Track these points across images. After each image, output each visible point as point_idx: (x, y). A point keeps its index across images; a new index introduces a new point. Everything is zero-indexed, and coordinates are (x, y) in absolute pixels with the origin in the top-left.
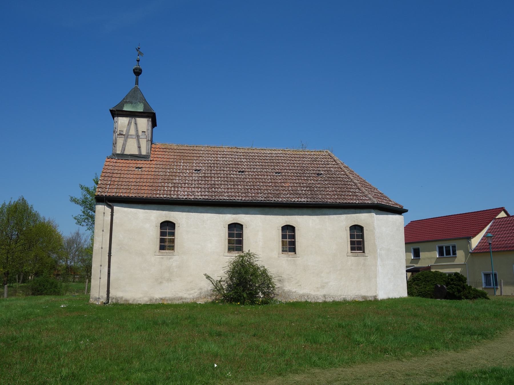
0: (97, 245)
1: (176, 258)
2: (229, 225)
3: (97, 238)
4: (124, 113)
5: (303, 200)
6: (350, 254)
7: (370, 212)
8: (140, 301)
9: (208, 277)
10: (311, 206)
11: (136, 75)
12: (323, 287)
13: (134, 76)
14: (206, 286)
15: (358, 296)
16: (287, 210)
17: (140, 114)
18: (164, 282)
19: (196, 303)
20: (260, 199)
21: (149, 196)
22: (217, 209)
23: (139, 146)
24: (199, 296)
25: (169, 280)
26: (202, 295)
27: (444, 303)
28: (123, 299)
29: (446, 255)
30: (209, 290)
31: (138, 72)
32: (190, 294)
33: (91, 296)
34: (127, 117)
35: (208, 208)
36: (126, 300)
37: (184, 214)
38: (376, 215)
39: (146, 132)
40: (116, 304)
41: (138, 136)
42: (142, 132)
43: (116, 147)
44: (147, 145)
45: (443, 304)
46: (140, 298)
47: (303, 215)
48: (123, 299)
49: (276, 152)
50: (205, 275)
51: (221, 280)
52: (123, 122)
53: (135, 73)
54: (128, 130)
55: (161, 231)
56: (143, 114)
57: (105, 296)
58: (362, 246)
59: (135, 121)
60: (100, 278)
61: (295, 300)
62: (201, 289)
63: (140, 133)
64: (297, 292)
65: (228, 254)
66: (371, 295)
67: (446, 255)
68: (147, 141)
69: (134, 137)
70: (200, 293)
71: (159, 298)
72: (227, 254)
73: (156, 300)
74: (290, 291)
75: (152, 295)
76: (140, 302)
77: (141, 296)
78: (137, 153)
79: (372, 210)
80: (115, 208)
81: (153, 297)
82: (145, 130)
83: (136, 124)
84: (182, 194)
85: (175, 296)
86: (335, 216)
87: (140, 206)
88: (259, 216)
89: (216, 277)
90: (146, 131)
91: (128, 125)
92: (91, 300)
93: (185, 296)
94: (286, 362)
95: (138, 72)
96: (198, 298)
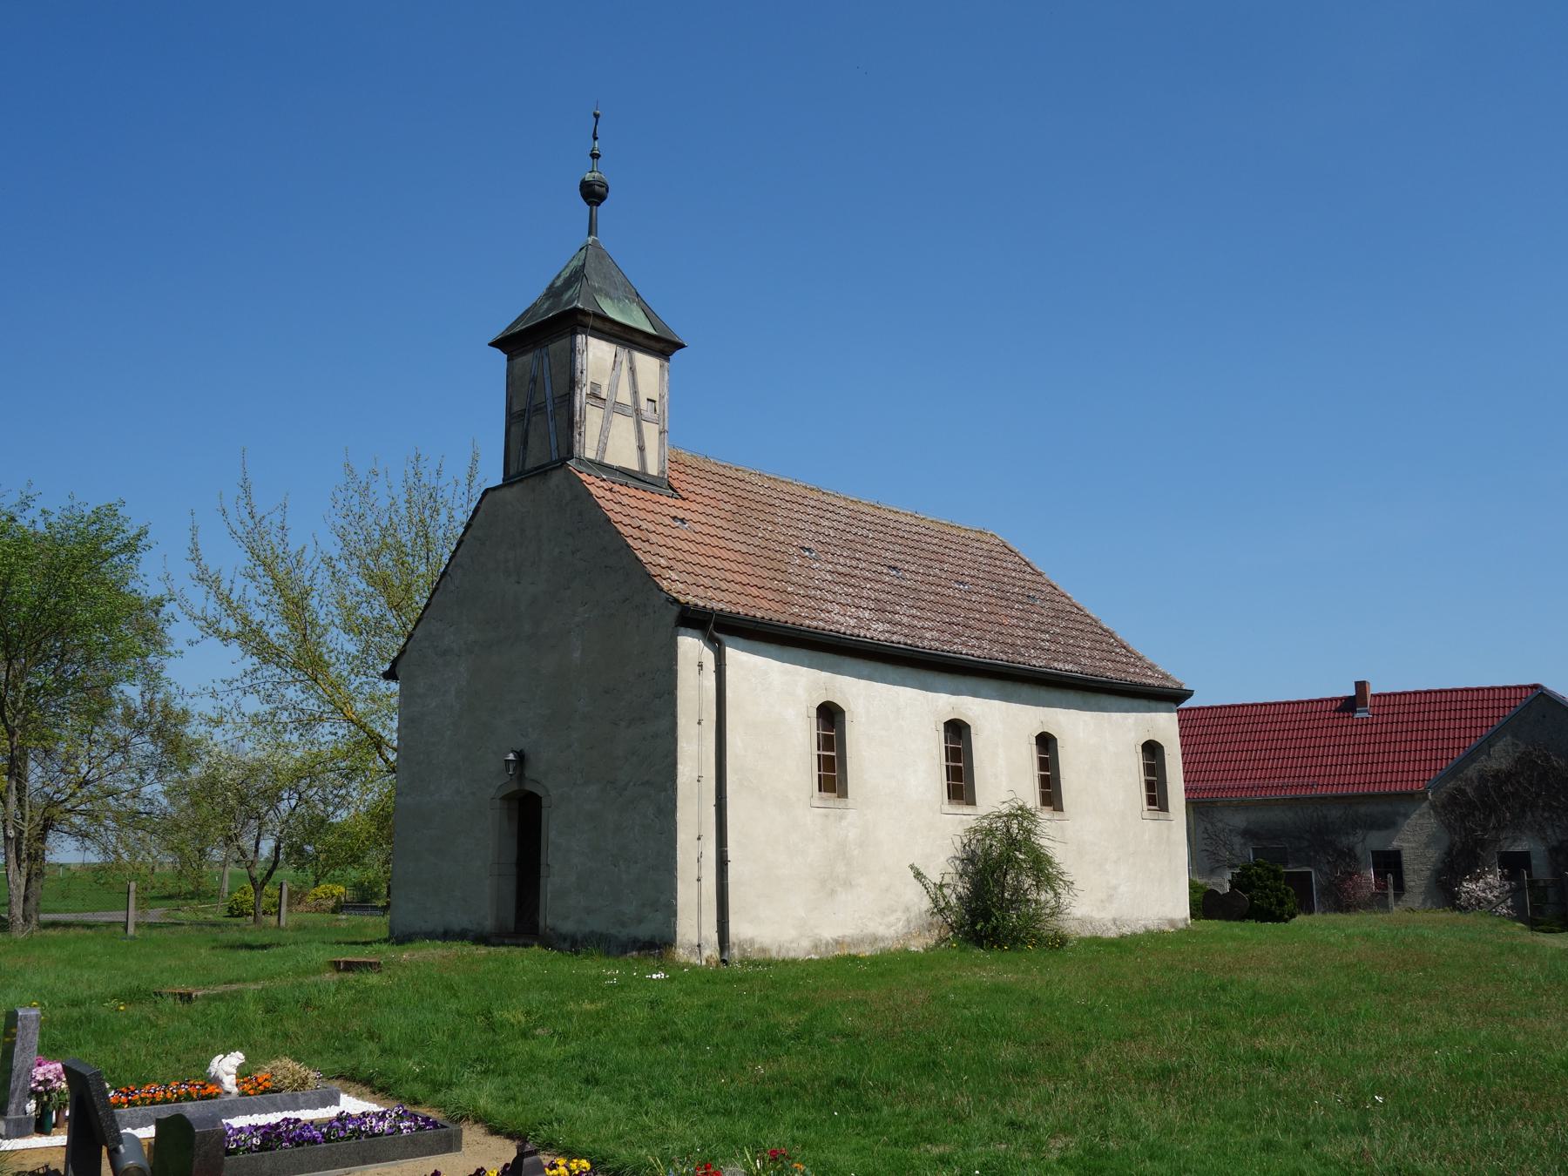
0: (686, 769)
1: (851, 815)
2: (945, 723)
3: (685, 745)
4: (607, 327)
5: (1060, 666)
6: (1147, 814)
8: (795, 951)
9: (918, 875)
10: (1093, 685)
11: (588, 204)
12: (1110, 898)
14: (916, 900)
16: (1043, 693)
17: (640, 339)
18: (839, 889)
19: (906, 951)
21: (776, 617)
23: (641, 444)
24: (905, 931)
25: (848, 884)
26: (912, 925)
27: (1237, 931)
28: (756, 946)
30: (923, 910)
31: (593, 194)
32: (889, 926)
33: (679, 938)
34: (611, 342)
36: (763, 950)
37: (863, 683)
39: (657, 403)
40: (746, 961)
41: (638, 411)
42: (648, 400)
43: (583, 434)
44: (660, 447)
46: (792, 942)
48: (756, 946)
49: (897, 517)
50: (912, 867)
51: (944, 883)
52: (599, 354)
54: (614, 386)
55: (1040, 758)
56: (652, 344)
57: (711, 934)
58: (1156, 794)
59: (631, 361)
60: (699, 880)
62: (907, 909)
63: (644, 405)
65: (950, 809)
68: (660, 433)
69: (630, 411)
70: (908, 921)
71: (832, 938)
72: (947, 808)
73: (827, 944)
75: (816, 931)
76: (792, 955)
77: (793, 933)
78: (636, 468)
80: (733, 654)
81: (818, 937)
82: (656, 398)
83: (632, 370)
84: (842, 620)
85: (863, 933)
86: (1118, 714)
87: (773, 648)
88: (996, 703)
89: (934, 877)
90: (657, 399)
91: (613, 369)
92: (680, 951)
93: (881, 931)
94: (38, 992)
95: (593, 194)
96: (908, 936)
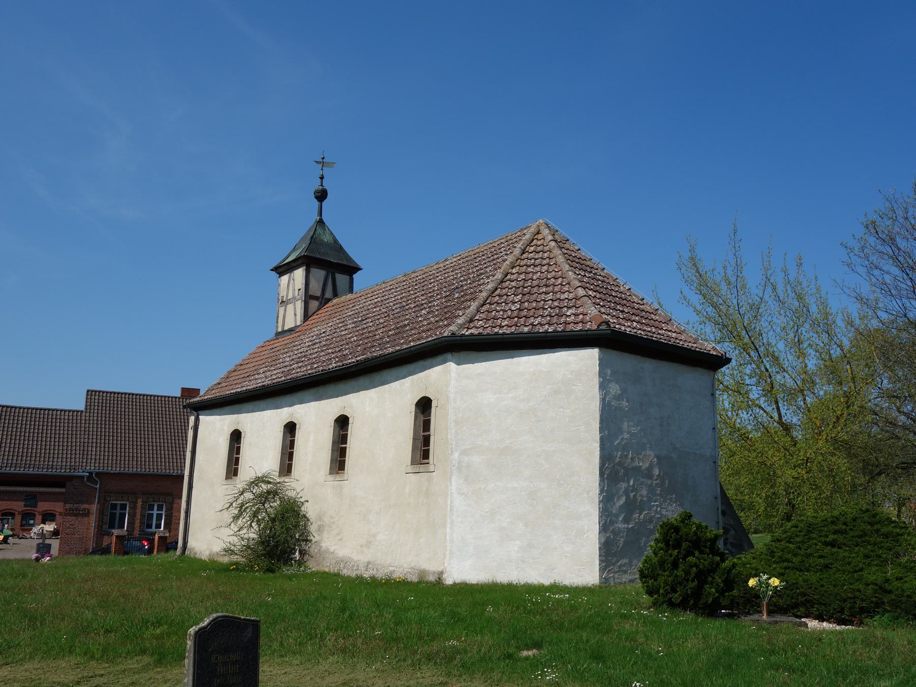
7: (445, 362)
12: (369, 544)
13: (317, 203)
15: (414, 569)
17: (294, 264)
20: (505, 330)
22: (331, 388)
29: (162, 511)
35: (261, 403)
38: (458, 364)
45: (803, 608)
47: (337, 397)
53: (317, 198)
61: (327, 570)
64: (336, 552)
66: (434, 569)
67: (162, 511)
74: (327, 551)
79: (449, 356)
95: (321, 196)
